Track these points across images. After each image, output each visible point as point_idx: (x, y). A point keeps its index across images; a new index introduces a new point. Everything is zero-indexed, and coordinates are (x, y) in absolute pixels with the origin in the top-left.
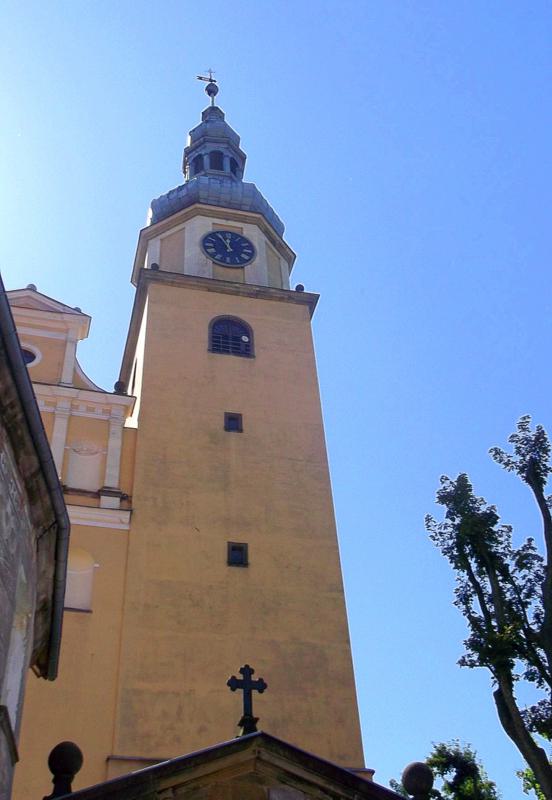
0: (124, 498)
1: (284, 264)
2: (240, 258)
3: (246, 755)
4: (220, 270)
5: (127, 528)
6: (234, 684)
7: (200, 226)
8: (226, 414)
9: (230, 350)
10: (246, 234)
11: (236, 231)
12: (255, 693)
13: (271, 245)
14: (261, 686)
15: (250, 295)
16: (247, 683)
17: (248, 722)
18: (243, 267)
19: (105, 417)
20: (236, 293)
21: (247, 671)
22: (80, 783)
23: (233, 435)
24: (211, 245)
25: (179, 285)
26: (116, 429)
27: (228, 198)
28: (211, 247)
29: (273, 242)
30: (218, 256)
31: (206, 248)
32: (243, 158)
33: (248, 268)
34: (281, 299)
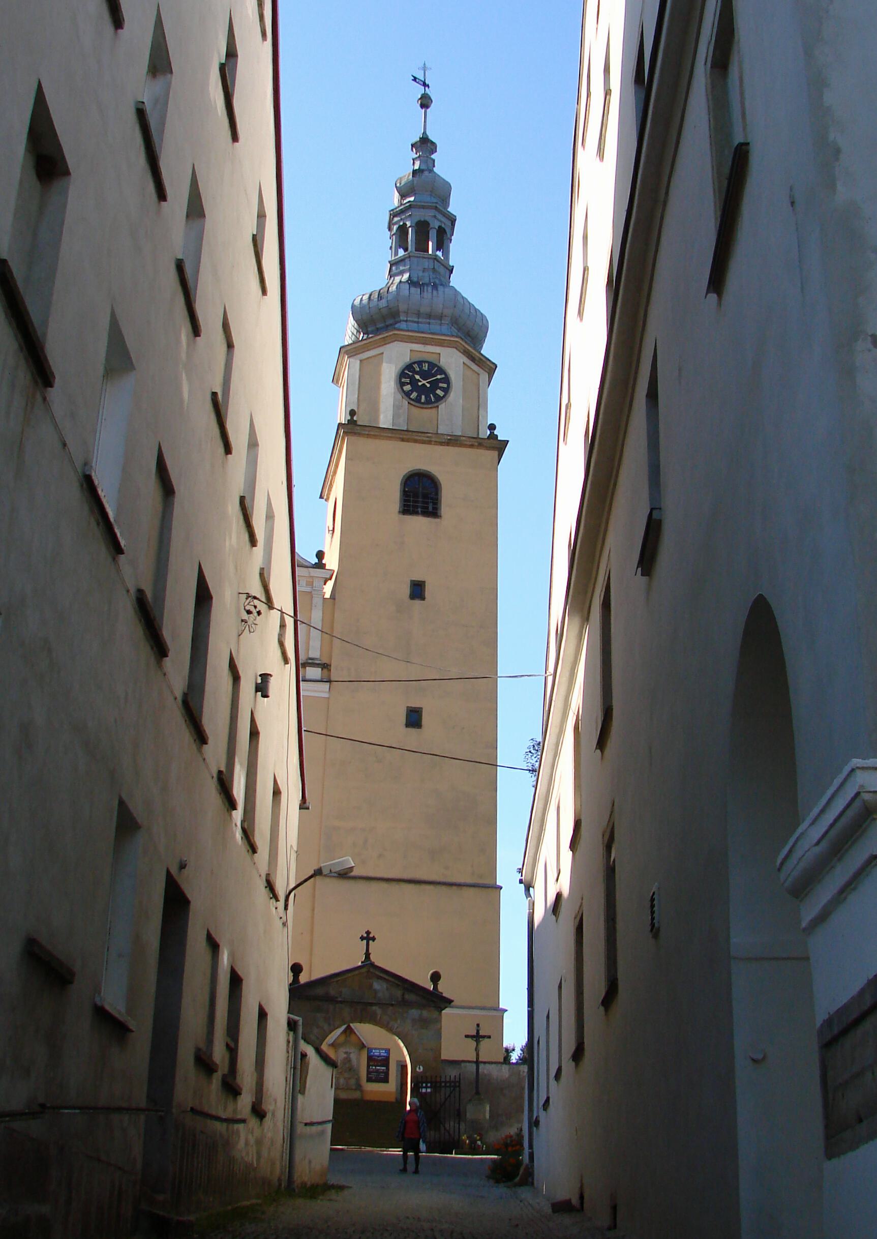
0: (325, 666)
1: (484, 376)
2: (436, 395)
3: (364, 970)
4: (416, 411)
5: (326, 695)
6: (362, 938)
7: (395, 356)
8: (412, 581)
9: (419, 510)
10: (443, 362)
11: (432, 359)
12: (371, 942)
13: (474, 367)
14: (374, 939)
15: (441, 444)
16: (368, 938)
17: (368, 955)
18: (438, 407)
19: (308, 589)
20: (429, 442)
21: (368, 933)
22: (303, 978)
23: (417, 602)
24: (408, 380)
25: (375, 437)
26: (317, 601)
27: (428, 310)
28: (408, 384)
29: (472, 358)
30: (414, 395)
31: (402, 384)
32: (453, 220)
33: (442, 406)
34: (472, 446)
